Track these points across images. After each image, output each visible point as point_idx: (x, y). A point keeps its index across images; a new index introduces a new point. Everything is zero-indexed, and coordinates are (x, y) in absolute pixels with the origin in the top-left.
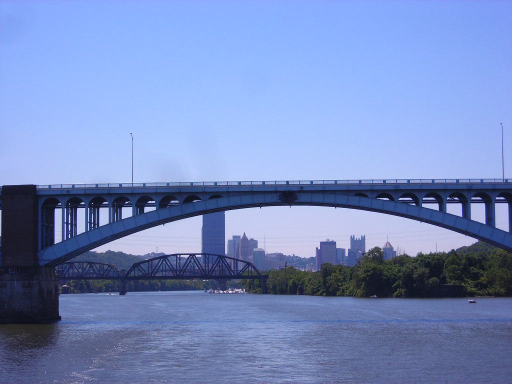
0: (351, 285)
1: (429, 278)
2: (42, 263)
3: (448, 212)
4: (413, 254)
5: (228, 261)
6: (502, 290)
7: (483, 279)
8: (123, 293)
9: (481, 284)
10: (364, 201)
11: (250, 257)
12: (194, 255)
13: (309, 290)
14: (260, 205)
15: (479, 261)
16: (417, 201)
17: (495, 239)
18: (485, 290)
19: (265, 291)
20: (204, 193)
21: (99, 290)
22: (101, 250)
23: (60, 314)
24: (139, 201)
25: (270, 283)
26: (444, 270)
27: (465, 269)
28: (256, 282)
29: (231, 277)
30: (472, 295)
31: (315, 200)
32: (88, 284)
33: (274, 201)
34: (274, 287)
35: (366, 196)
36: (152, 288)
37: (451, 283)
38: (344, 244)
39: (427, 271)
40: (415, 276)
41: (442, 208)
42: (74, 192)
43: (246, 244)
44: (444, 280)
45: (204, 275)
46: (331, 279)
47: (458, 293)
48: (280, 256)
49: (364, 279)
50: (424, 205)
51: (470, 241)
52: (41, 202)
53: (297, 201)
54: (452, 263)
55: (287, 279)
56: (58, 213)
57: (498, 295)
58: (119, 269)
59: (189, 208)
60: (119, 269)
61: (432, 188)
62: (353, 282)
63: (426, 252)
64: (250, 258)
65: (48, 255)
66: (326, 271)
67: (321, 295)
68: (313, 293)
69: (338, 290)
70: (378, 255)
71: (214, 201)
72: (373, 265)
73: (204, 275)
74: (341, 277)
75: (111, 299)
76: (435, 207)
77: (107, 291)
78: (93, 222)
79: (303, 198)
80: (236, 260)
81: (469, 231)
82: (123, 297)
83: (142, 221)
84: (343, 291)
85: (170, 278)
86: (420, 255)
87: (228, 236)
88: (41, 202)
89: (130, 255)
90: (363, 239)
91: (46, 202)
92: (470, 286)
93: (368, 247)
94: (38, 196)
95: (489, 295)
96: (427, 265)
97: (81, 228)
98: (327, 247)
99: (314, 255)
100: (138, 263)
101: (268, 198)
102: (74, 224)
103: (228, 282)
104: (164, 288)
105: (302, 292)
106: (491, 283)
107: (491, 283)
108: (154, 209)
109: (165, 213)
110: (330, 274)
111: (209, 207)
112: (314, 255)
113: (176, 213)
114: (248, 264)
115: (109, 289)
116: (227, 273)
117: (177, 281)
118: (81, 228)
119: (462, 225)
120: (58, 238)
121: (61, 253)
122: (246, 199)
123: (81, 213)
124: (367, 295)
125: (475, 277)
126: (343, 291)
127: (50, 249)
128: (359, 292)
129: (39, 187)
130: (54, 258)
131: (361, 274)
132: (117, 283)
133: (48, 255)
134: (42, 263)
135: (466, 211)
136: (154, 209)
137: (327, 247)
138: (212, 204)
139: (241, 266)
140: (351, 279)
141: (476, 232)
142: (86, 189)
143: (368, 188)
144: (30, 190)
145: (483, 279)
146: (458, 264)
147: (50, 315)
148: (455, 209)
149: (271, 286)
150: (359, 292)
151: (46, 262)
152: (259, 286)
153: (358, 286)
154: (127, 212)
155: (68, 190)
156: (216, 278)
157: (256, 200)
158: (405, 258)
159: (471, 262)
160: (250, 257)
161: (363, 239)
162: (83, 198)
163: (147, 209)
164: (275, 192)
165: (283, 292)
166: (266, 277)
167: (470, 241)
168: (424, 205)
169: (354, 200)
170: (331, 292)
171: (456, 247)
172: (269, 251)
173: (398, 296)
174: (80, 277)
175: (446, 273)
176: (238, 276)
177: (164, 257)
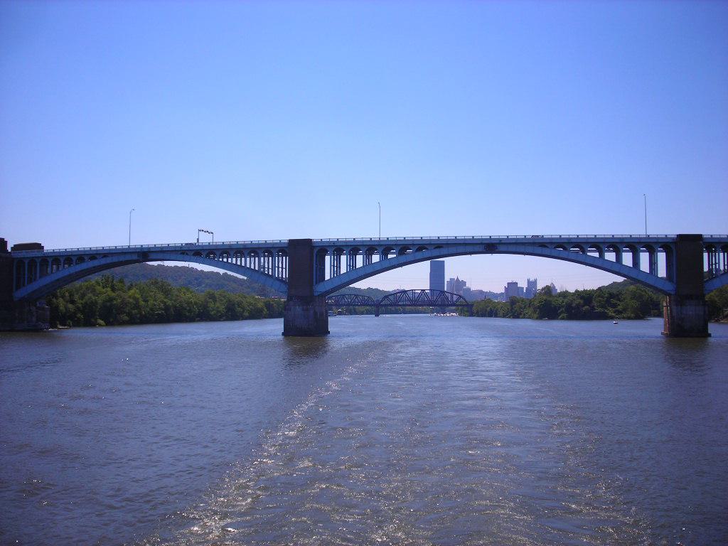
0: (529, 311)
1: (584, 306)
2: (316, 294)
3: (606, 258)
4: (572, 290)
5: (447, 294)
6: (632, 315)
7: (620, 308)
8: (377, 315)
9: (618, 311)
10: (546, 251)
11: (461, 292)
12: (424, 290)
13: (501, 314)
14: (471, 253)
15: (617, 295)
16: (584, 251)
17: (640, 278)
18: (621, 314)
19: (472, 315)
20: (430, 244)
21: (362, 313)
22: (357, 285)
23: (709, 332)
24: (384, 250)
25: (474, 309)
26: (594, 302)
27: (608, 301)
28: (465, 309)
29: (450, 305)
30: (612, 318)
31: (510, 250)
32: (354, 309)
33: (481, 250)
34: (477, 312)
35: (548, 247)
36: (396, 312)
37: (599, 310)
38: (523, 284)
39: (582, 302)
40: (574, 305)
41: (601, 255)
42: (338, 244)
43: (458, 284)
44: (593, 308)
45: (431, 303)
46: (516, 307)
47: (603, 317)
48: (481, 292)
49: (539, 307)
50: (589, 254)
51: (620, 279)
52: (316, 250)
53: (497, 250)
54: (599, 296)
55: (487, 307)
56: (327, 258)
57: (629, 318)
58: (375, 300)
59: (419, 255)
60: (375, 300)
61: (438, 242)
62: (531, 309)
63: (581, 289)
64: (461, 293)
65: (320, 288)
66: (513, 302)
67: (509, 317)
68: (504, 316)
69: (521, 314)
70: (548, 290)
71: (437, 250)
72: (544, 298)
73: (431, 303)
74: (523, 306)
75: (369, 321)
76: (597, 255)
77: (367, 314)
78: (352, 265)
79: (502, 248)
80: (452, 294)
81: (621, 272)
82: (377, 318)
83: (386, 264)
84: (524, 315)
85: (409, 305)
86: (577, 291)
87: (447, 279)
88: (316, 250)
89: (585, 291)
90: (536, 281)
91: (319, 251)
92: (610, 312)
93: (540, 286)
94: (314, 247)
95: (624, 318)
96: (582, 298)
97: (343, 270)
98: (512, 286)
99: (503, 291)
100: (387, 295)
101: (477, 249)
102: (339, 267)
103: (447, 309)
104: (405, 312)
105: (496, 316)
106: (625, 310)
107: (625, 310)
108: (395, 256)
109: (403, 259)
110: (515, 304)
111: (434, 254)
112: (503, 291)
113: (410, 258)
114: (460, 296)
115: (368, 313)
116: (446, 303)
117: (412, 308)
118: (343, 270)
119: (615, 268)
120: (327, 277)
121: (328, 287)
122: (461, 249)
123: (343, 258)
124: (541, 317)
125: (614, 306)
126: (524, 315)
127: (321, 284)
128: (536, 316)
129: (705, 237)
130: (324, 290)
131: (536, 303)
132: (374, 308)
133: (320, 288)
134: (316, 294)
135: (619, 258)
136: (395, 256)
137: (512, 286)
138: (436, 252)
139: (455, 298)
140: (530, 307)
141: (626, 273)
142: (346, 242)
143: (548, 241)
144: (308, 242)
145: (620, 308)
146: (602, 297)
147: (321, 330)
148: (610, 256)
149: (475, 311)
150: (536, 316)
151: (319, 293)
152: (467, 311)
153: (535, 312)
154: (376, 258)
155: (334, 242)
156: (440, 305)
157: (468, 250)
158: (565, 294)
159: (611, 296)
160: (461, 292)
161: (536, 281)
162: (344, 248)
163: (390, 256)
164: (482, 244)
165: (483, 315)
166: (472, 305)
167: (620, 279)
168: (589, 254)
169: (539, 250)
170: (516, 316)
171: (606, 284)
172: (473, 288)
173: (563, 319)
174: (349, 305)
175: (595, 303)
176: (454, 305)
177: (404, 292)
